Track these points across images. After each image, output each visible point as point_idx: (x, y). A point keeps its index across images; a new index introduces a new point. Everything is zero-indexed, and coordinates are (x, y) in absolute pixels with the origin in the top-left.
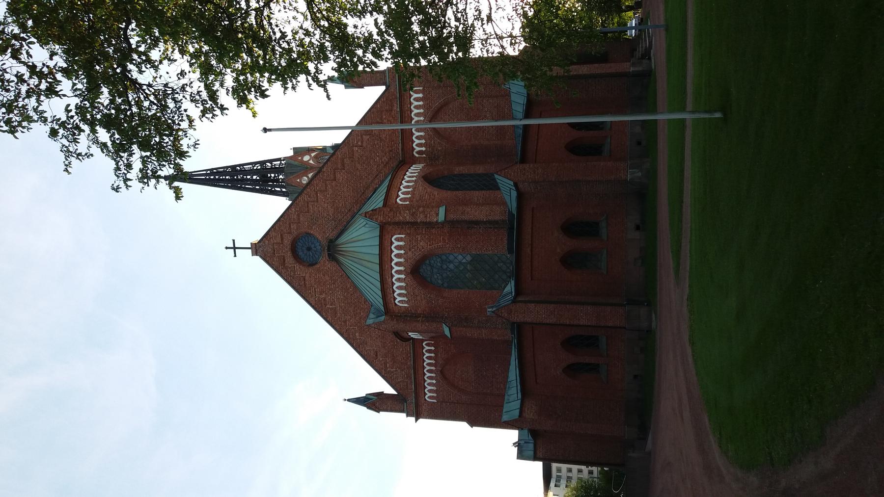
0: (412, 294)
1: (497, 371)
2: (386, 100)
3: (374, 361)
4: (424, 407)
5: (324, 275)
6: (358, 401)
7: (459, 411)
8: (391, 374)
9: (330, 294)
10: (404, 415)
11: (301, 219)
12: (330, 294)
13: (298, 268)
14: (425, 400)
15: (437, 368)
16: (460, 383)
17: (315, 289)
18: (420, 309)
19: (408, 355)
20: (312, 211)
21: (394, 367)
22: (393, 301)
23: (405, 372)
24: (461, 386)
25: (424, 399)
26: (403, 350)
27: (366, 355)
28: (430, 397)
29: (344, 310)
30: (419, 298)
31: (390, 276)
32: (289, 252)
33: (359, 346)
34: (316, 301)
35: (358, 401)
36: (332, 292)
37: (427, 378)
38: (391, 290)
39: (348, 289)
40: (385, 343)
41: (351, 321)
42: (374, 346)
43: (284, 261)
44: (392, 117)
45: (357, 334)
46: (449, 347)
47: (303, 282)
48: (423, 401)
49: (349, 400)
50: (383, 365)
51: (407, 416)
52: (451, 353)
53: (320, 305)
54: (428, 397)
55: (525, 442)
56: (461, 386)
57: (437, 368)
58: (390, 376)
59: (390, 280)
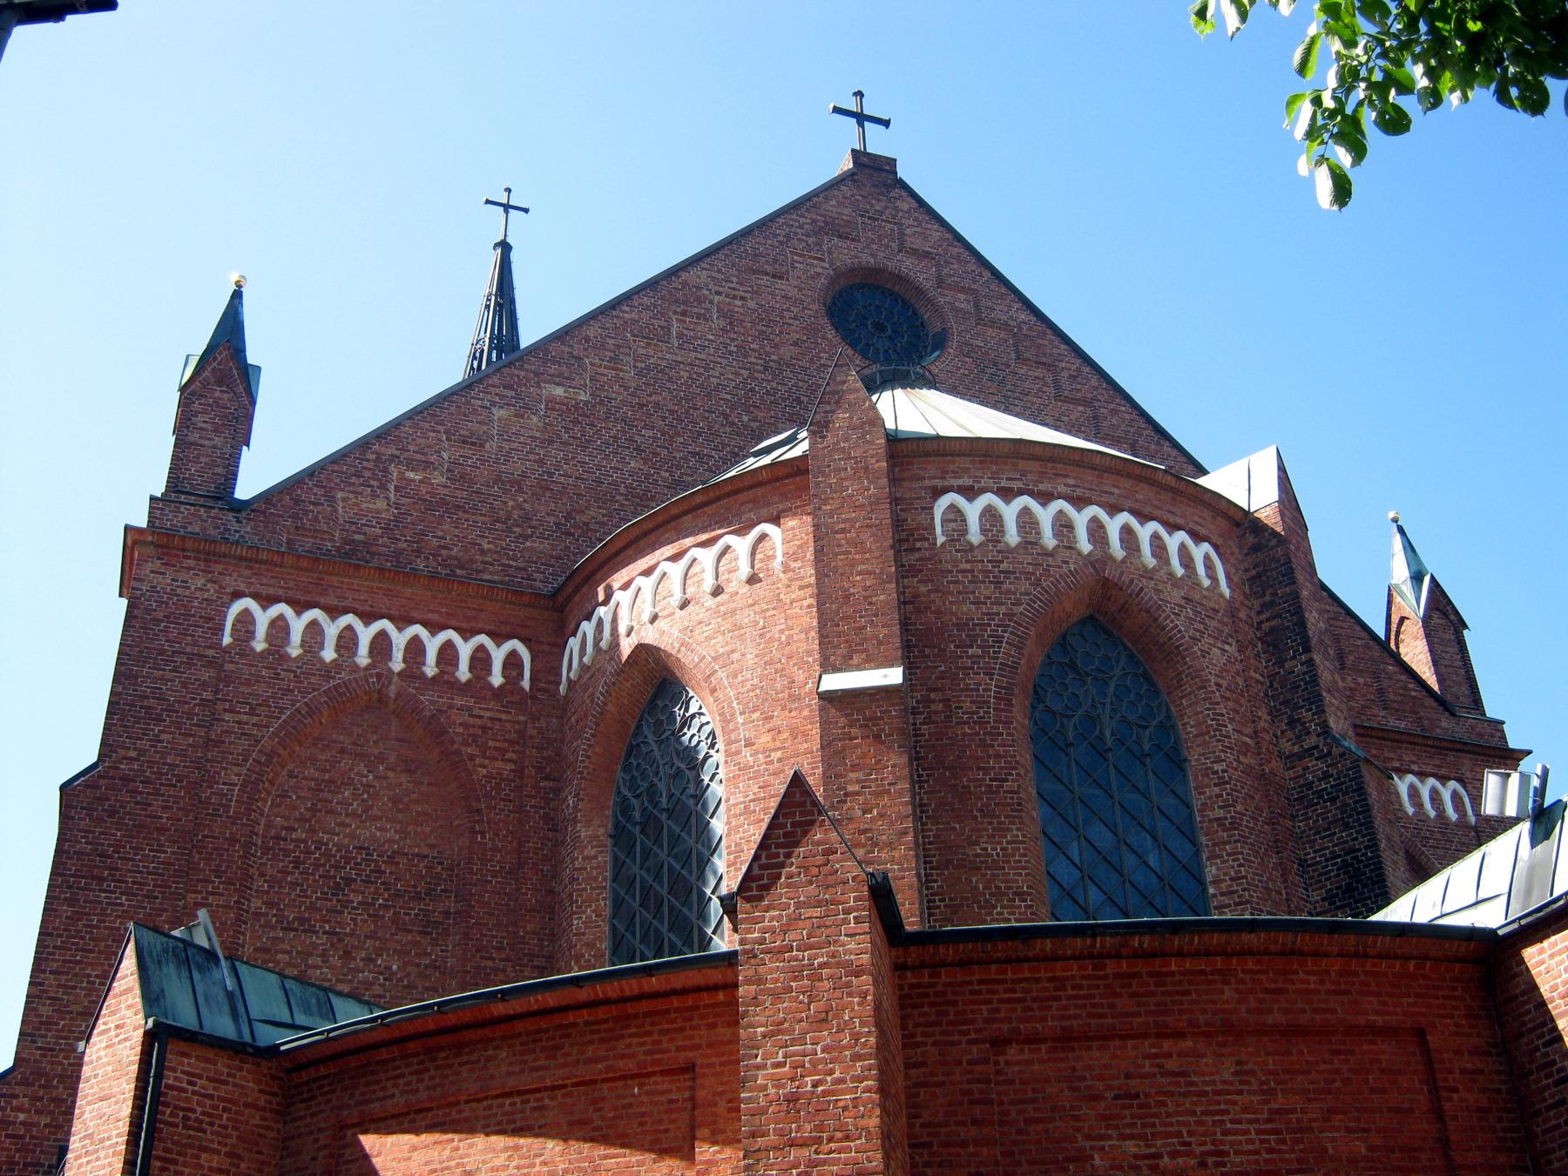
0: (1003, 566)
1: (369, 960)
2: (1414, 698)
3: (442, 429)
4: (200, 582)
5: (796, 344)
6: (230, 330)
7: (164, 737)
8: (375, 476)
9: (726, 345)
10: (159, 491)
11: (990, 332)
12: (726, 345)
13: (819, 270)
14: (238, 595)
15: (395, 679)
16: (310, 772)
17: (742, 298)
18: (923, 589)
19: (462, 568)
20: (1022, 371)
21: (403, 500)
22: (960, 482)
23: (376, 538)
24: (291, 775)
25: (242, 587)
26: (483, 552)
27: (469, 403)
28: (246, 619)
29: (662, 371)
30: (985, 590)
31: (1079, 492)
32: (872, 261)
33: (510, 387)
34: (700, 288)
35: (230, 330)
36: (731, 353)
37: (349, 628)
38: (1015, 485)
39: (748, 412)
40: (520, 490)
41: (616, 388)
42: (506, 446)
43: (840, 237)
44: (1364, 707)
45: (559, 391)
46: (503, 751)
47: (769, 268)
48: (231, 583)
49: (237, 295)
50: (419, 456)
51: (152, 499)
52: (472, 757)
53: (680, 295)
54: (246, 612)
55: (230, 995)
56: (291, 775)
57: (395, 679)
58: (367, 474)
59: (1061, 489)
